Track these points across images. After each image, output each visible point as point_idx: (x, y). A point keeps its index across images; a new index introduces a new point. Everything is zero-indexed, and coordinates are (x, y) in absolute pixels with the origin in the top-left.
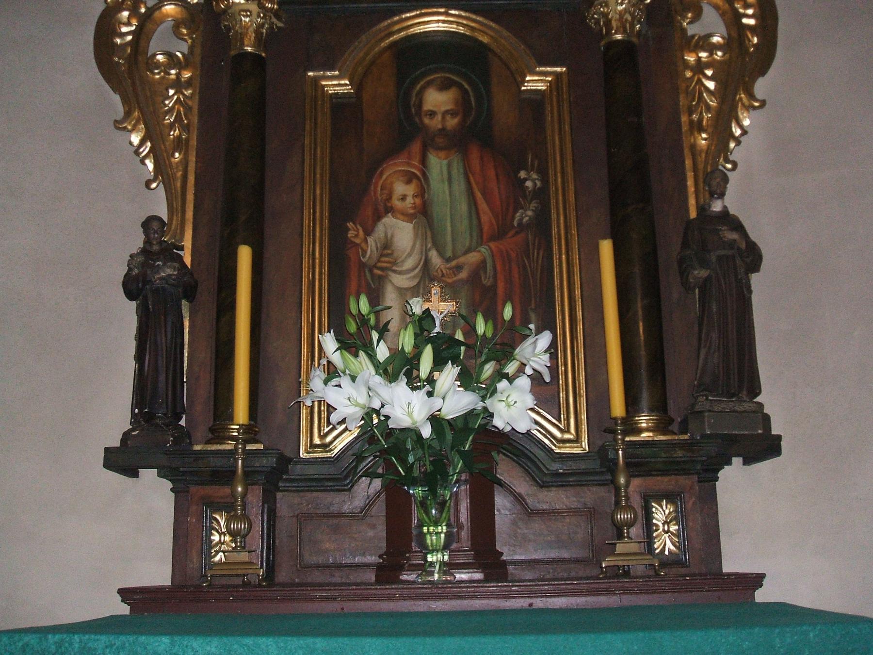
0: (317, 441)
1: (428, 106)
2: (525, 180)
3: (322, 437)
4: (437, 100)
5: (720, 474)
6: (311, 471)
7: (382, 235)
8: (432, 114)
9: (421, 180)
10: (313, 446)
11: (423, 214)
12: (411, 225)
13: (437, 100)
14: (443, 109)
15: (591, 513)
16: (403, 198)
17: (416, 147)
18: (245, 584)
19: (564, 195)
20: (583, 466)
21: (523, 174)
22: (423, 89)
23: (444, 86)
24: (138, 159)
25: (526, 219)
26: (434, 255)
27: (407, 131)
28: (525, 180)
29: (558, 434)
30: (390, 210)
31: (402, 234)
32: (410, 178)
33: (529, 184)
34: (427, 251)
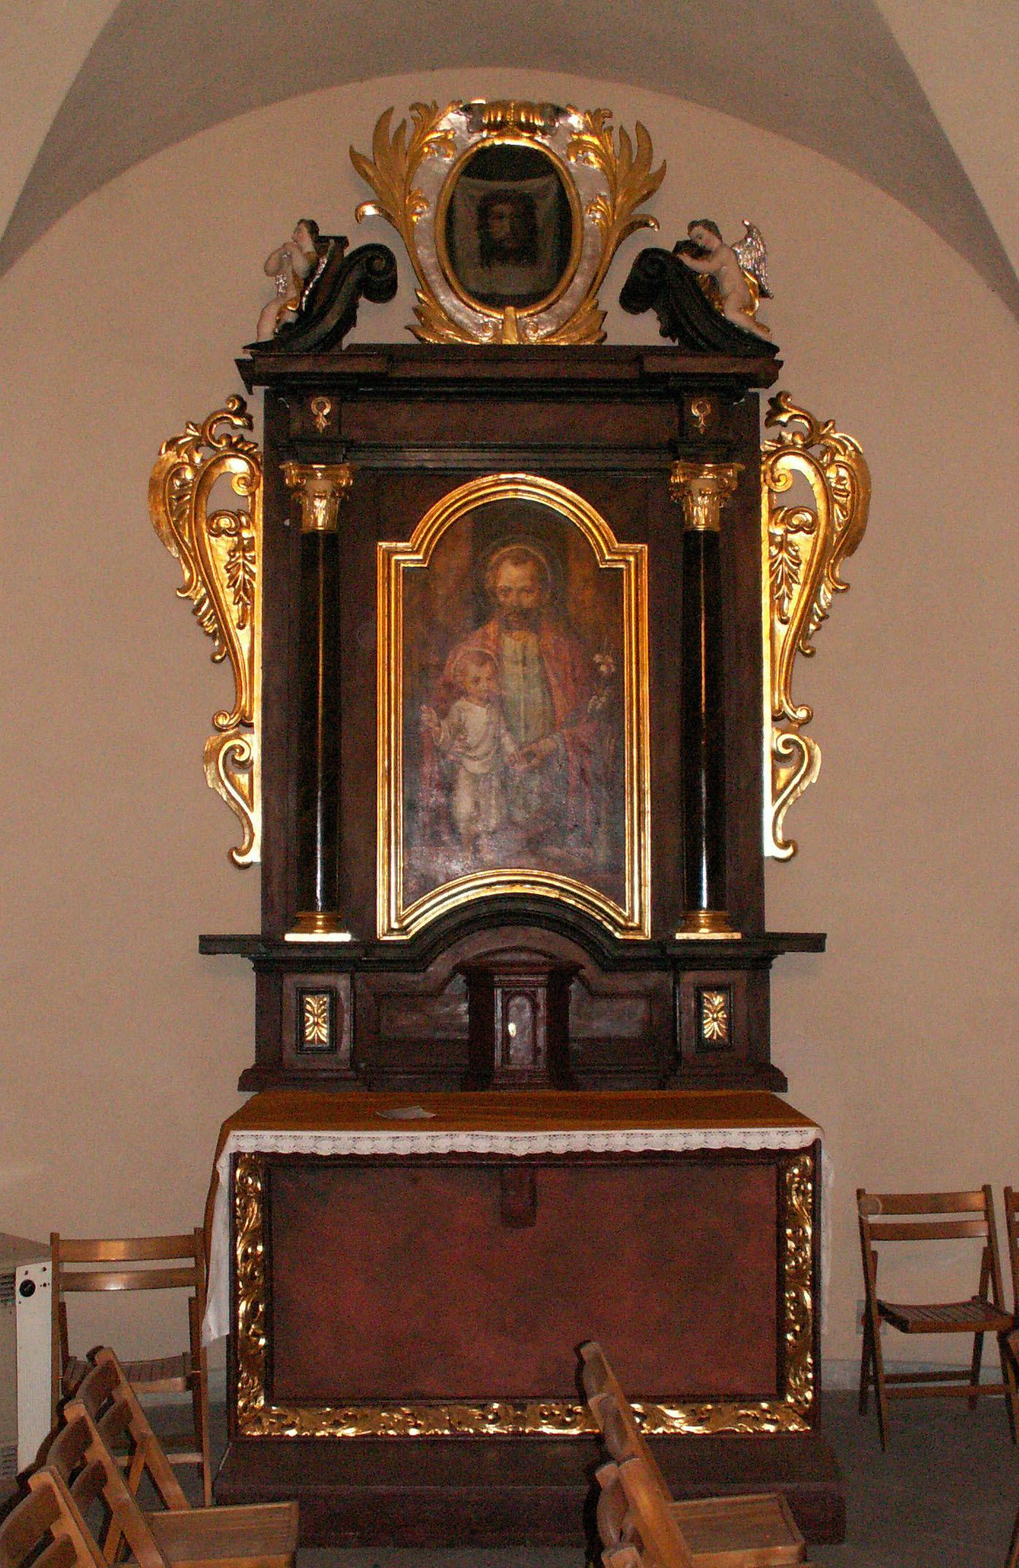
0: (395, 925)
1: (502, 583)
2: (599, 664)
3: (400, 920)
4: (511, 576)
5: (774, 962)
6: (390, 955)
7: (456, 720)
8: (508, 590)
9: (492, 659)
10: (391, 930)
11: (499, 703)
12: (484, 710)
13: (511, 576)
14: (520, 585)
15: (650, 996)
16: (477, 680)
17: (491, 628)
18: (784, 1216)
19: (638, 690)
20: (644, 952)
21: (597, 658)
22: (498, 564)
23: (517, 562)
24: (195, 619)
25: (599, 707)
26: (507, 740)
27: (482, 605)
28: (599, 664)
29: (622, 921)
30: (463, 693)
31: (476, 716)
32: (483, 659)
33: (603, 668)
34: (315, 317)
